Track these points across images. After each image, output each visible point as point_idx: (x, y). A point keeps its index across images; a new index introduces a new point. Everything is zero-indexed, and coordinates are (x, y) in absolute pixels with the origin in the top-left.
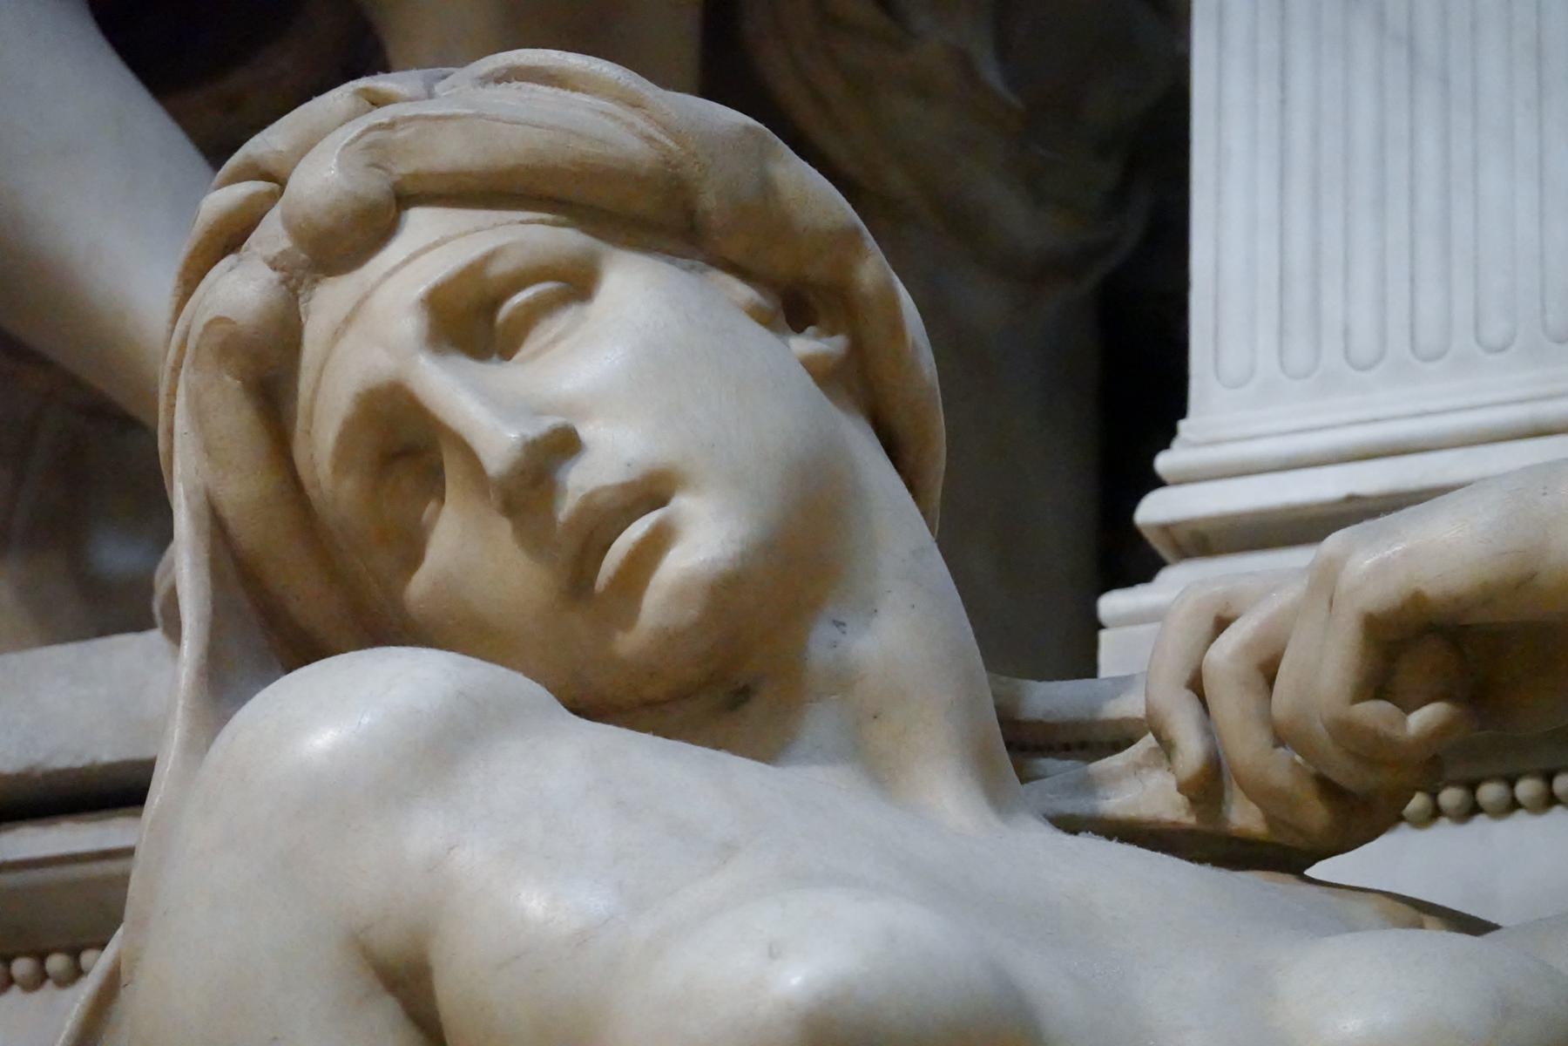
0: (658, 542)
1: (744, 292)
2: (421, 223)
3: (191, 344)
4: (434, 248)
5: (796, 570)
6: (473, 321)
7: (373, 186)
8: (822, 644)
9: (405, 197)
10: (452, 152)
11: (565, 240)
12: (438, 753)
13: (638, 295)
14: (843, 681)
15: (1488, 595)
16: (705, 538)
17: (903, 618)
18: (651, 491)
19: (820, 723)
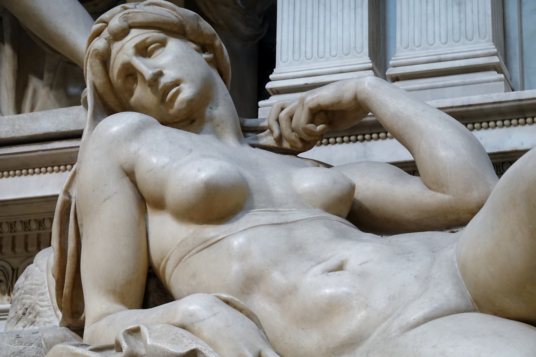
1: (194, 46)
2: (134, 32)
4: (136, 36)
6: (143, 50)
7: (125, 25)
10: (140, 19)
11: (161, 35)
13: (174, 46)
14: (212, 119)
15: (332, 105)
16: (186, 92)
17: (223, 107)
18: (176, 83)
19: (207, 127)
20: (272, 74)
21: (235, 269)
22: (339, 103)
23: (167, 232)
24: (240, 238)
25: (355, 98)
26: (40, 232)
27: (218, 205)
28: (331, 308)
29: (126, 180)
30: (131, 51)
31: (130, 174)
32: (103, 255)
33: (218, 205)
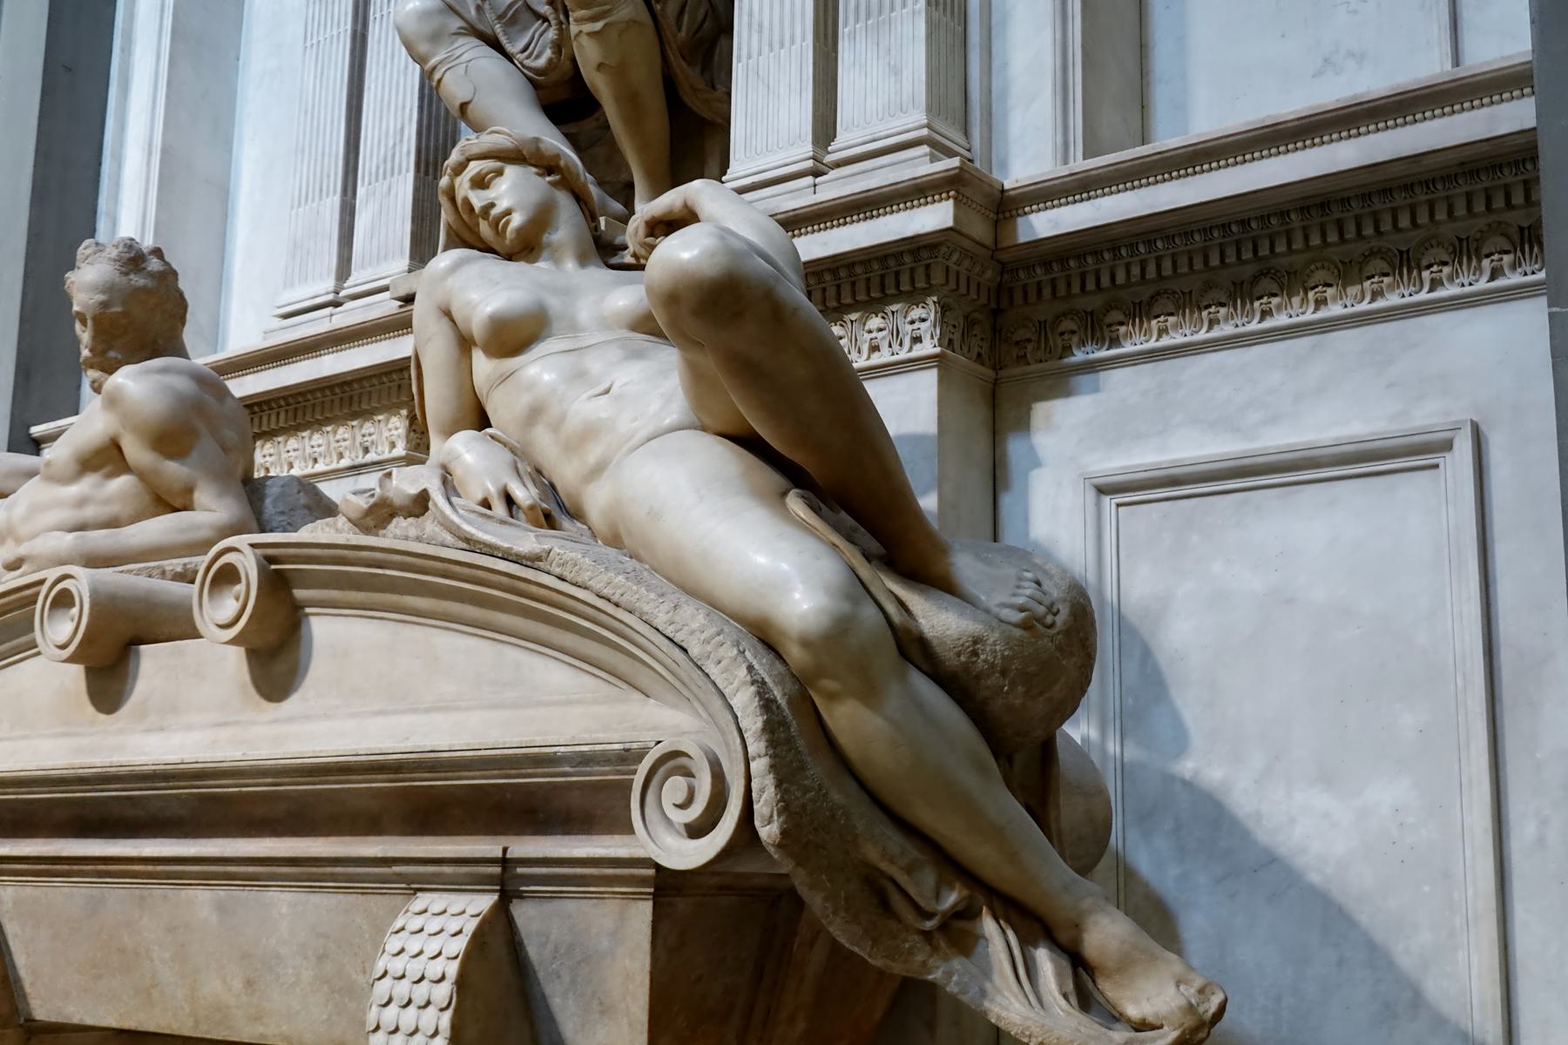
0: (508, 223)
1: (534, 170)
2: (472, 164)
3: (596, 10)
4: (474, 167)
5: (541, 220)
6: (480, 183)
7: (462, 158)
8: (546, 238)
9: (469, 160)
10: (475, 150)
11: (499, 164)
12: (455, 267)
13: (511, 171)
14: (549, 245)
15: (665, 215)
16: (517, 220)
17: (566, 228)
18: (508, 212)
19: (545, 254)
20: (72, 266)
21: (525, 400)
22: (671, 212)
23: (483, 366)
24: (539, 369)
25: (685, 205)
26: (1429, 197)
27: (514, 336)
28: (589, 433)
29: (446, 319)
30: (466, 185)
31: (448, 314)
32: (437, 396)
33: (514, 336)
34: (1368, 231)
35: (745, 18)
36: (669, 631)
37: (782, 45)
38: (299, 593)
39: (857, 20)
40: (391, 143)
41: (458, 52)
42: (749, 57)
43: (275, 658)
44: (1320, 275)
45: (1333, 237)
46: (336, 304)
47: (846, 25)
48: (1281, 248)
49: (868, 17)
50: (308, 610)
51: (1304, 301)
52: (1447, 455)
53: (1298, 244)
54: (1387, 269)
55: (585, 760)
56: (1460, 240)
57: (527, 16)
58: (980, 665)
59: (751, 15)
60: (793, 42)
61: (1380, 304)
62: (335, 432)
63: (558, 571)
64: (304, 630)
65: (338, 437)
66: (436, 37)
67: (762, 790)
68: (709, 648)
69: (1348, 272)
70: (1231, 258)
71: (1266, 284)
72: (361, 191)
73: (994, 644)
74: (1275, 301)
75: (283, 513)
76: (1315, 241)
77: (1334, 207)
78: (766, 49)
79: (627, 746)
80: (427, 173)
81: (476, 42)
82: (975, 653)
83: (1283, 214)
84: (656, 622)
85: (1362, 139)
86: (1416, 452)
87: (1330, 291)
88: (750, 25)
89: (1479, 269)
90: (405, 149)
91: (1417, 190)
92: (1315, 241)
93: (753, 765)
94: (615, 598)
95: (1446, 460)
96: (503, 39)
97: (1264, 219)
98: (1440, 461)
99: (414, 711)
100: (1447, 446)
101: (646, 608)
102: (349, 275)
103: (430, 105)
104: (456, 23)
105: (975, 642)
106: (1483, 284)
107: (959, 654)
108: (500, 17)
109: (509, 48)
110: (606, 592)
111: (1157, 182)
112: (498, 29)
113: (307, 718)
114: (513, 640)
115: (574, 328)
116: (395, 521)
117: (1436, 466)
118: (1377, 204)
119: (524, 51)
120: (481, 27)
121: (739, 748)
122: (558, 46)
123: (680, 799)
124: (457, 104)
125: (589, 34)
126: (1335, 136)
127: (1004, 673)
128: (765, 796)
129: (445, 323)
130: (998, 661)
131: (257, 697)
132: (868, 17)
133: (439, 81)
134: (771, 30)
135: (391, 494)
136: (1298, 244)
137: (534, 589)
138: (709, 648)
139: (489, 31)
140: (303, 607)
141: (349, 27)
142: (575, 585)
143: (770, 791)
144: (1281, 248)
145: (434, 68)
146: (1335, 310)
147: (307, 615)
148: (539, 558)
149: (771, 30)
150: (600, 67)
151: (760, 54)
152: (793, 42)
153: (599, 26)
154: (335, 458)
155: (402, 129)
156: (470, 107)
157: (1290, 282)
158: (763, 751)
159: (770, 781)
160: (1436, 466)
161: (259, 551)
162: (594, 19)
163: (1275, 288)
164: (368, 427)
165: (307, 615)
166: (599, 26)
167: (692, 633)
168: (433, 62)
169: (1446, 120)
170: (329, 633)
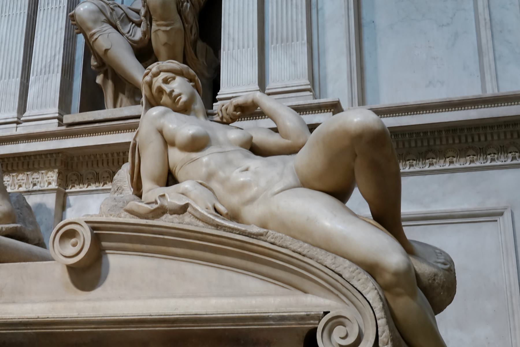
0: (180, 99)
1: (187, 79)
2: (162, 73)
4: (163, 75)
5: (191, 101)
6: (166, 81)
9: (160, 72)
10: (164, 68)
11: (173, 75)
12: (163, 114)
13: (178, 79)
14: (194, 110)
15: (244, 104)
16: (184, 98)
17: (199, 105)
18: (180, 95)
19: (192, 113)
22: (246, 103)
23: (176, 156)
24: (206, 158)
25: (253, 102)
27: (197, 145)
28: (243, 186)
31: (161, 132)
32: (150, 165)
33: (197, 145)
34: (470, 140)
35: (227, 36)
36: (333, 267)
37: (243, 47)
38: (104, 244)
39: (277, 43)
40: (49, 61)
41: (105, 29)
42: (228, 50)
43: (87, 274)
44: (450, 153)
45: (457, 141)
46: (18, 123)
47: (272, 43)
48: (438, 142)
49: (282, 42)
50: (107, 251)
51: (445, 161)
52: (501, 218)
53: (444, 142)
54: (475, 154)
55: (282, 318)
56: (501, 146)
57: (126, 20)
58: (436, 284)
59: (229, 34)
60: (248, 47)
61: (472, 165)
62: (17, 176)
63: (272, 240)
64: (104, 260)
65: (19, 178)
66: (95, 22)
67: (384, 332)
68: (354, 274)
69: (462, 153)
70: (419, 144)
71: (430, 154)
72: (32, 78)
73: (441, 276)
74: (434, 160)
75: (18, 209)
76: (451, 141)
77: (458, 131)
78: (236, 48)
79: (308, 313)
80: (65, 75)
81: (111, 27)
82: (434, 280)
83: (440, 131)
84: (325, 263)
85: (479, 110)
86: (492, 216)
87: (455, 159)
88: (229, 38)
89: (486, 158)
90: (56, 64)
91: (488, 129)
92: (451, 141)
93: (378, 322)
94: (304, 253)
95: (500, 219)
96: (120, 27)
97: (432, 132)
98: (498, 219)
99: (174, 297)
100: (501, 214)
101: (320, 257)
102: (25, 111)
103: (67, 47)
104: (103, 18)
105: (435, 276)
106: (509, 162)
107: (429, 280)
108: (119, 18)
109: (122, 31)
110: (299, 250)
111: (399, 116)
112: (118, 22)
113: (108, 299)
114: (229, 268)
115: (219, 144)
116: (165, 216)
117: (496, 221)
118: (473, 132)
119: (128, 32)
120: (111, 20)
121: (373, 315)
122: (144, 34)
123: (343, 335)
124: (104, 49)
125: (164, 31)
126: (470, 108)
127: (442, 287)
128: (384, 335)
129: (159, 136)
130: (441, 283)
131: (75, 289)
132: (282, 42)
133: (96, 39)
134: (238, 41)
135: (166, 204)
136: (444, 142)
137: (255, 248)
138: (354, 274)
139: (114, 23)
140: (104, 250)
141: (26, 11)
142: (279, 246)
143: (387, 332)
144: (438, 142)
145: (94, 34)
146: (457, 165)
147: (107, 253)
148: (261, 235)
149: (238, 41)
150: (165, 44)
151: (233, 49)
152: (248, 47)
153: (168, 28)
154: (17, 186)
155: (55, 56)
156: (109, 51)
157: (442, 154)
158: (383, 316)
159: (387, 328)
160: (496, 221)
161: (90, 225)
162: (167, 26)
163: (434, 156)
164: (36, 175)
165: (107, 253)
166: (168, 28)
167: (345, 268)
168: (93, 31)
169: (508, 107)
170: (116, 261)
